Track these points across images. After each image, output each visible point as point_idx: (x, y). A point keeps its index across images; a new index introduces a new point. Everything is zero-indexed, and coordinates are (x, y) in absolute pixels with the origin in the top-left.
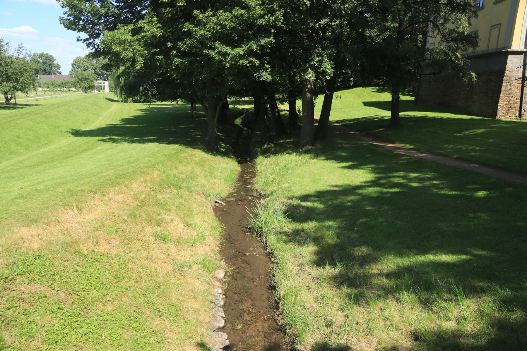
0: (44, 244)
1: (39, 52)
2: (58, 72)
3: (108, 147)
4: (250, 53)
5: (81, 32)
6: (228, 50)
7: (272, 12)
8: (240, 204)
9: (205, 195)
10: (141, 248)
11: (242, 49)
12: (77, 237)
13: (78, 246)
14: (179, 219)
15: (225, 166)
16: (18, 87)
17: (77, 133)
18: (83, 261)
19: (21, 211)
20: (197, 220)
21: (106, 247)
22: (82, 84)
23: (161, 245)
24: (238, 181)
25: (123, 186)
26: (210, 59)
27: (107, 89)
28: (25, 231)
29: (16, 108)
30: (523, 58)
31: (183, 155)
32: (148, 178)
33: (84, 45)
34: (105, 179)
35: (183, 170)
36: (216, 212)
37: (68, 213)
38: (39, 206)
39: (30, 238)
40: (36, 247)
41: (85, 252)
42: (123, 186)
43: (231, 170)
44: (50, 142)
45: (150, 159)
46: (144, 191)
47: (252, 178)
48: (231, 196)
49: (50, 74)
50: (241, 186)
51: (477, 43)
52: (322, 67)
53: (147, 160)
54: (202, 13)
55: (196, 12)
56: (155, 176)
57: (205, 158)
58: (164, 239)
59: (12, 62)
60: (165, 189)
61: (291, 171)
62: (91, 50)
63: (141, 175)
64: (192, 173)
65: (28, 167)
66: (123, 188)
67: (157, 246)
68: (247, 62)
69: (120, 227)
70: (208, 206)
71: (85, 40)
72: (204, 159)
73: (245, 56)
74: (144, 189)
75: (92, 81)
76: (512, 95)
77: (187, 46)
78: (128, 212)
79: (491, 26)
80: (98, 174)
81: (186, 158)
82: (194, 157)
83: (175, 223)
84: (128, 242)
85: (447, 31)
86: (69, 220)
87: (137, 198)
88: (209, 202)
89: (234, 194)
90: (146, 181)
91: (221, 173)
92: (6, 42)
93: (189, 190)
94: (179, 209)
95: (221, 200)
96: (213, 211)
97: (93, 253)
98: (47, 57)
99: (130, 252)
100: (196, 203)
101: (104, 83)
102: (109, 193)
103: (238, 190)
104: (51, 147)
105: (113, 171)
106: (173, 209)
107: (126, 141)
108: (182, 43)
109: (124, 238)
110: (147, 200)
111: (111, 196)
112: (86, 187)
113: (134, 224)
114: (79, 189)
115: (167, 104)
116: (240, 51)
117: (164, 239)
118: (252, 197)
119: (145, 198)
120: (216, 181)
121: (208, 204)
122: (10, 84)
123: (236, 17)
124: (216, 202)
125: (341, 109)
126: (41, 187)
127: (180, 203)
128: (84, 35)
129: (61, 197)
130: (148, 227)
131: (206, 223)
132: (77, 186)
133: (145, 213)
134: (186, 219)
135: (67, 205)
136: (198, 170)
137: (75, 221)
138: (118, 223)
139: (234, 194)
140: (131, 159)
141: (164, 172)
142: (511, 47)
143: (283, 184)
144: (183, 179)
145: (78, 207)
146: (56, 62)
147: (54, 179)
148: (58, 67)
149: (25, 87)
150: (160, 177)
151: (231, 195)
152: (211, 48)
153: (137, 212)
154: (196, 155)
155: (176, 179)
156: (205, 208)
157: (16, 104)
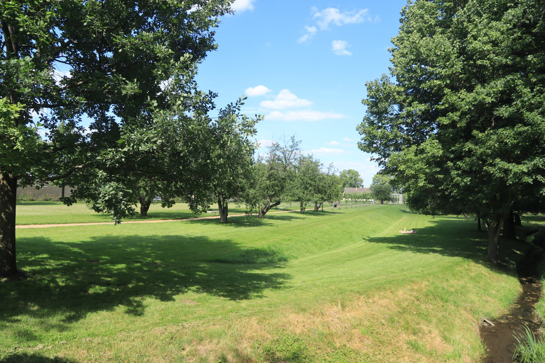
0: (305, 330)
1: (347, 169)
2: (361, 185)
3: (388, 254)
5: (375, 153)
8: (513, 328)
9: (473, 311)
10: (390, 352)
12: (334, 331)
13: (333, 339)
14: (438, 332)
15: (503, 284)
16: (325, 198)
17: (372, 240)
18: (333, 352)
19: (297, 300)
20: (457, 336)
21: (358, 344)
22: (380, 196)
23: (412, 354)
24: (517, 303)
25: (389, 291)
26: (489, 175)
27: (401, 202)
28: (292, 317)
29: (323, 215)
31: (458, 269)
32: (415, 287)
33: (377, 163)
34: (374, 282)
35: (455, 283)
36: (482, 332)
37: (333, 308)
38: (311, 299)
39: (296, 323)
40: (298, 331)
41: (338, 345)
42: (389, 291)
43: (509, 290)
44: (340, 245)
45: (424, 269)
46: (409, 299)
48: (504, 318)
49: (354, 187)
50: (519, 308)
53: (420, 269)
54: (481, 132)
55: (475, 132)
56: (423, 286)
57: (483, 274)
58: (415, 347)
59: (323, 178)
60: (430, 300)
62: (382, 167)
63: (409, 283)
64: (463, 288)
65: (316, 264)
66: (388, 293)
67: (408, 354)
68: (532, 180)
69: (375, 329)
70: (473, 324)
71: (377, 160)
72: (481, 275)
73: (529, 174)
74: (409, 297)
75: (388, 194)
77: (467, 165)
78: (387, 316)
80: (370, 278)
81: (461, 272)
82: (469, 272)
83: (433, 335)
84: (380, 345)
86: (332, 314)
87: (400, 305)
88: (475, 320)
89: (509, 317)
90: (412, 290)
91: (497, 291)
92: (321, 163)
94: (440, 321)
96: (478, 330)
97: (344, 347)
98: (353, 173)
99: (380, 354)
101: (398, 196)
102: (374, 296)
103: (514, 313)
104: (339, 250)
105: (384, 277)
106: (434, 320)
107: (411, 250)
108: (461, 162)
109: (376, 340)
110: (409, 308)
111: (376, 299)
112: (356, 288)
113: (390, 328)
114: (349, 288)
115: (452, 218)
116: (523, 168)
117: (415, 347)
118: (530, 322)
119: (408, 306)
120: (489, 299)
121: (474, 322)
122: (319, 195)
123: (520, 134)
124: (485, 321)
126: (318, 283)
128: (376, 156)
129: (332, 294)
130: (404, 334)
131: (467, 341)
132: (348, 286)
133: (404, 320)
134: (445, 333)
135: (333, 301)
136: (470, 285)
137: (337, 316)
138: (375, 324)
139: (509, 317)
140: (405, 267)
141: (433, 283)
144: (452, 293)
145: (342, 305)
146: (360, 177)
147: (332, 277)
148: (362, 181)
149: (331, 197)
150: (427, 288)
151: (504, 317)
152: (491, 165)
153: (396, 318)
154: (472, 270)
155: (443, 292)
156: (470, 326)
157: (322, 211)
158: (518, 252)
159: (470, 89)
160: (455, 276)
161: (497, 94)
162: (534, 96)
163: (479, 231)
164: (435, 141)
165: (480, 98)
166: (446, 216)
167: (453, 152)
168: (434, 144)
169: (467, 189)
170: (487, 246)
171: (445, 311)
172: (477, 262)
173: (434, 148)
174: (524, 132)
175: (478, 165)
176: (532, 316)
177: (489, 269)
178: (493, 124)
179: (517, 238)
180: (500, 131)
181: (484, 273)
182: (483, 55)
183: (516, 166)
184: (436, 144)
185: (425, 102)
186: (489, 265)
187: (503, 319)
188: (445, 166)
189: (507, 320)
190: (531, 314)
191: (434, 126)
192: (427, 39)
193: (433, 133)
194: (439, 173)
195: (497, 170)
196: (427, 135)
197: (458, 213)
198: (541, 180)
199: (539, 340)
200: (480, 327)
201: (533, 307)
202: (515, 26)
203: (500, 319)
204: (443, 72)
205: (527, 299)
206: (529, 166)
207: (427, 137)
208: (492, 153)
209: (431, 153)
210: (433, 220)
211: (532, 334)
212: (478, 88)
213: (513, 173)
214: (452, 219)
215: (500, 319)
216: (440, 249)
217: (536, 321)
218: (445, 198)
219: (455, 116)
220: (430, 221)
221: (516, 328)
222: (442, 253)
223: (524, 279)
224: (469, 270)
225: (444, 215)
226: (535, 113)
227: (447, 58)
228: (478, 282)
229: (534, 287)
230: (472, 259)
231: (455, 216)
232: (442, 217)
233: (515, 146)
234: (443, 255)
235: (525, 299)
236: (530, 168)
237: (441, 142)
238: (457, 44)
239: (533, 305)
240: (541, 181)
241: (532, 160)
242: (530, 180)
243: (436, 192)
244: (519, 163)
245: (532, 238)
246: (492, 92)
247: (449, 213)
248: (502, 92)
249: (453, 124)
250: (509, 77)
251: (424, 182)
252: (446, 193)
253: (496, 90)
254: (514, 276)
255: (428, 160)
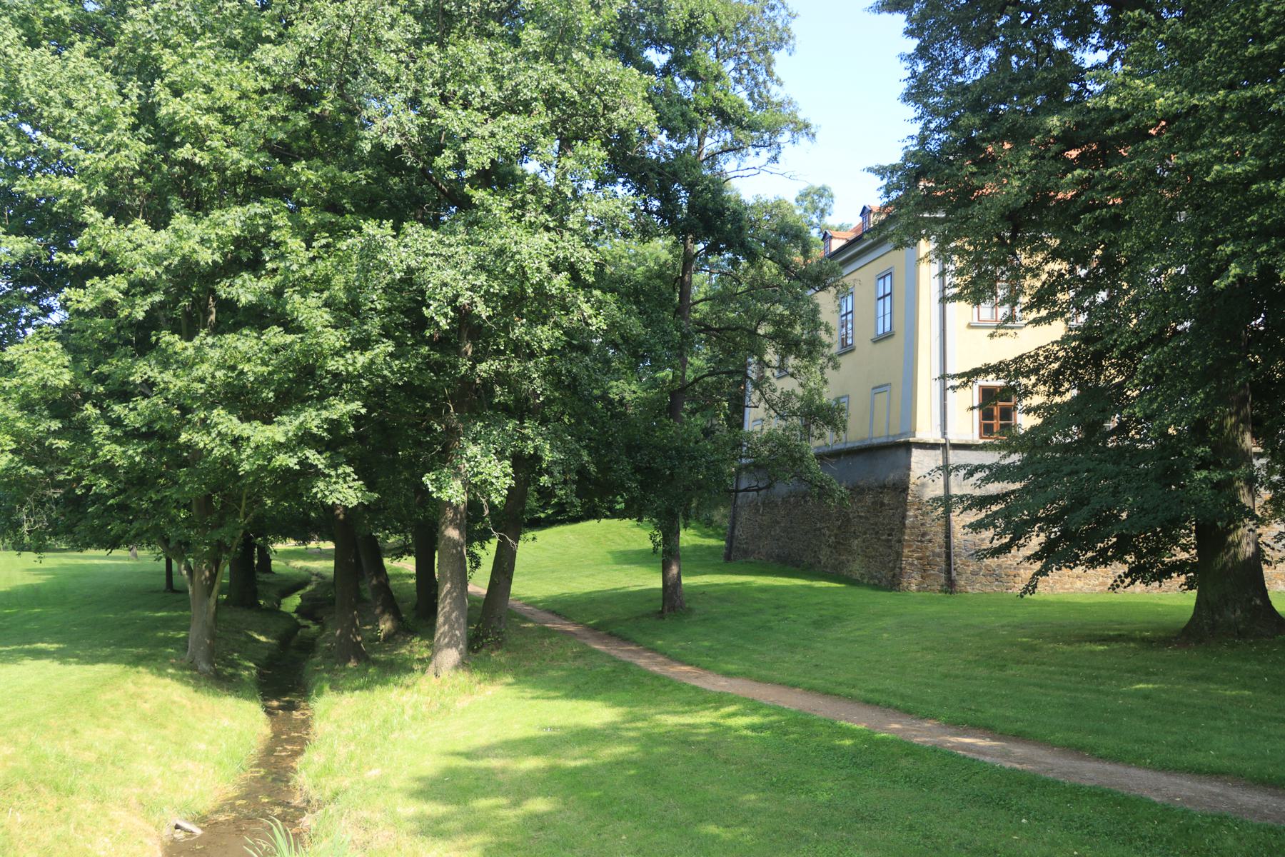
4: (305, 439)
6: (244, 429)
7: (362, 344)
8: (246, 830)
9: (147, 807)
11: (282, 428)
15: (226, 722)
24: (258, 765)
26: (198, 454)
30: (941, 457)
31: (109, 696)
47: (296, 754)
48: (227, 807)
50: (263, 777)
51: (844, 422)
52: (482, 473)
55: (167, 337)
57: (174, 702)
60: (19, 797)
61: (396, 734)
64: (121, 746)
68: (296, 460)
70: (146, 840)
76: (928, 537)
79: (873, 389)
81: (115, 706)
85: (778, 394)
88: (152, 829)
93: (98, 797)
95: (194, 822)
100: (110, 832)
103: (250, 794)
108: (125, 407)
115: (95, 558)
116: (277, 432)
121: (148, 835)
124: (177, 827)
125: (553, 572)
127: (58, 838)
141: (31, 746)
142: (914, 433)
143: (370, 769)
150: (10, 764)
154: (147, 697)
158: (263, 639)
159: (159, 220)
160: (98, 719)
161: (225, 244)
162: (313, 260)
163: (171, 590)
164: (51, 343)
165: (187, 246)
166: (79, 554)
167: (101, 379)
168: (48, 351)
169: (138, 479)
170: (187, 628)
171: (66, 821)
172: (160, 673)
173: (46, 362)
174: (285, 347)
175: (170, 418)
176: (289, 791)
177: (190, 689)
178: (213, 317)
179: (262, 602)
180: (230, 338)
181: (177, 699)
182: (199, 138)
183: (260, 428)
184: (53, 354)
185: (29, 232)
186: (192, 677)
187: (223, 811)
188: (79, 416)
189: (232, 811)
190: (288, 786)
191: (53, 302)
192: (43, 54)
193: (49, 321)
194: (58, 434)
195: (214, 439)
196: (29, 324)
197: (113, 544)
198: (316, 462)
199: (303, 843)
200: (163, 844)
201: (292, 768)
202: (277, 88)
203: (217, 812)
204: (88, 160)
205: (280, 751)
206: (289, 428)
207: (30, 331)
208: (207, 392)
209: (35, 377)
210: (38, 565)
211: (287, 835)
212: (181, 220)
213: (252, 445)
214: (96, 562)
215: (217, 812)
216: (56, 646)
217: (297, 800)
218: (75, 504)
219: (112, 287)
220: (28, 570)
221: (252, 828)
222: (61, 656)
223: (275, 703)
224: (139, 696)
225: (72, 549)
226: (314, 300)
227: (105, 122)
228: (163, 726)
229: (296, 720)
230: (147, 666)
231: (103, 552)
232: (67, 557)
233: (264, 381)
234: (63, 662)
235: (275, 751)
236: (290, 434)
237: (67, 348)
238: (133, 88)
239: (293, 764)
240: (317, 465)
241: (297, 416)
242: (292, 462)
243: (47, 486)
244: (267, 421)
245: (292, 603)
246: (213, 236)
247: (88, 546)
248: (238, 242)
249: (108, 308)
250: (256, 208)
251: (10, 456)
252: (79, 492)
253: (224, 232)
254: (251, 698)
255: (26, 395)
